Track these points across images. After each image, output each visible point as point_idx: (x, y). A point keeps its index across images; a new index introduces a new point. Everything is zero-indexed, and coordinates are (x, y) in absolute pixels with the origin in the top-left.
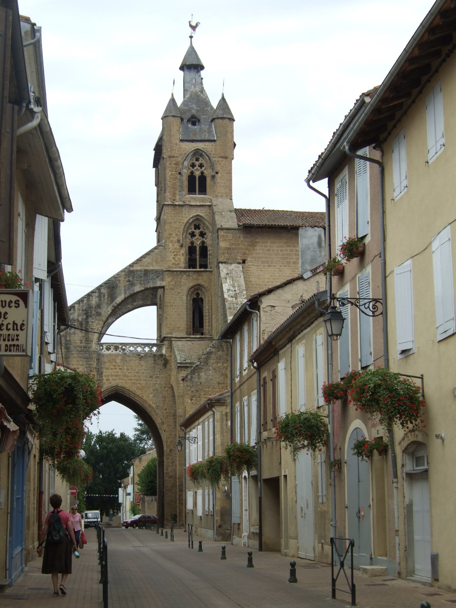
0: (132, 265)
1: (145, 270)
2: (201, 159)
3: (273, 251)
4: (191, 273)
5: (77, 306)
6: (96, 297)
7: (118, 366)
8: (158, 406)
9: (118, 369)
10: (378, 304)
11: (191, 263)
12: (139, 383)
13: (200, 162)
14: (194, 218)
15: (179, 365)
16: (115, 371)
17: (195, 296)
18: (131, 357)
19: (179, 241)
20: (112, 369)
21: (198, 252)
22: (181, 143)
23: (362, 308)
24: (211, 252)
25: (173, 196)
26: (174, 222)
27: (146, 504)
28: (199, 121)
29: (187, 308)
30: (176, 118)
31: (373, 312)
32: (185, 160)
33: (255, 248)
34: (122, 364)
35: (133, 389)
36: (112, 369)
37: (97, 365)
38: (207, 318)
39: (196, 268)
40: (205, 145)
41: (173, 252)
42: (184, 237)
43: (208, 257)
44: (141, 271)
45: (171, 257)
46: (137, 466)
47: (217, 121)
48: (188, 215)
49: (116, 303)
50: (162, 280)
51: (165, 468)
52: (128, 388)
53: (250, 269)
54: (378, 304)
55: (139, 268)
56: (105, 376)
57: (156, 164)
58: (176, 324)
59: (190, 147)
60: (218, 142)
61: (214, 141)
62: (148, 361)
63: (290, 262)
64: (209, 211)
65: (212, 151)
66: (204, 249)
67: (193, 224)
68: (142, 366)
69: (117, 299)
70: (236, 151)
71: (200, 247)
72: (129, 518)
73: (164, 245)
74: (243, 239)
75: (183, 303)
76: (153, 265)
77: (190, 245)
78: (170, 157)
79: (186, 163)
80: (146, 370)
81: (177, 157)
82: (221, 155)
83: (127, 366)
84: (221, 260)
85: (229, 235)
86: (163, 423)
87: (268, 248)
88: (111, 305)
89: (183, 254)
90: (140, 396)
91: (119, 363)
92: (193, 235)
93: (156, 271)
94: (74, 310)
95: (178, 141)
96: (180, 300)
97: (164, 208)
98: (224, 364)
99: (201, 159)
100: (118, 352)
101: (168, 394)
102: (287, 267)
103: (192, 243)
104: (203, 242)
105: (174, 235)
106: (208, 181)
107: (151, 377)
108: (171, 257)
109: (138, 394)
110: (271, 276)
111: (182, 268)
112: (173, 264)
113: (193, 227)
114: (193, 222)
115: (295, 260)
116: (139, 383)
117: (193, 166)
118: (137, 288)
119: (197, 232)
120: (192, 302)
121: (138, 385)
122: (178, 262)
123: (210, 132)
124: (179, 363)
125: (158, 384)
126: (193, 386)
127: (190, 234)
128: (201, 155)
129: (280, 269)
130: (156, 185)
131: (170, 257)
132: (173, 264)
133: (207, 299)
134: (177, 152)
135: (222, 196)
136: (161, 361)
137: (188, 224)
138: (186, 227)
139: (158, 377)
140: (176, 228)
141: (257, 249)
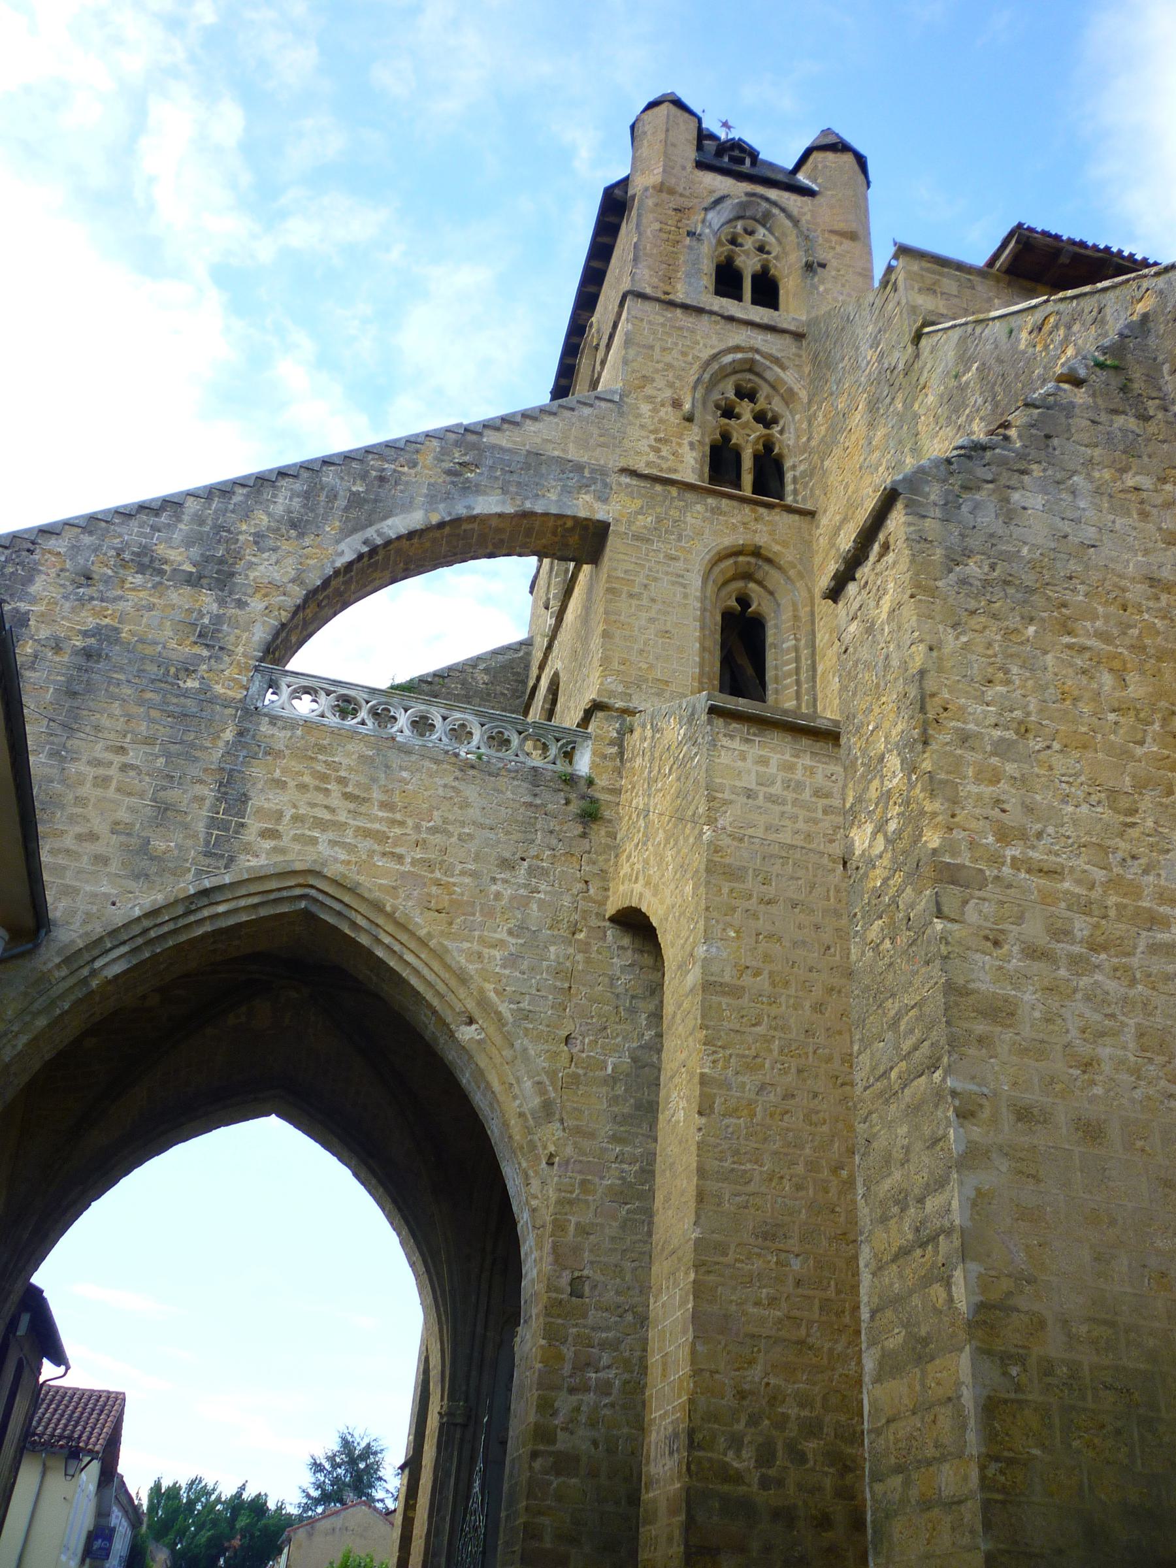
5: (192, 506)
7: (342, 781)
16: (320, 798)
29: (702, 620)
34: (363, 780)
35: (405, 905)
36: (303, 787)
46: (300, 1546)
49: (379, 534)
52: (377, 895)
56: (259, 811)
58: (651, 667)
62: (499, 791)
67: (733, 378)
68: (464, 805)
69: (389, 522)
75: (686, 596)
80: (482, 826)
82: (836, 228)
89: (691, 444)
90: (432, 943)
92: (729, 413)
96: (674, 583)
100: (351, 722)
101: (588, 961)
107: (507, 864)
109: (422, 933)
120: (719, 618)
125: (541, 902)
133: (786, 615)
139: (545, 873)
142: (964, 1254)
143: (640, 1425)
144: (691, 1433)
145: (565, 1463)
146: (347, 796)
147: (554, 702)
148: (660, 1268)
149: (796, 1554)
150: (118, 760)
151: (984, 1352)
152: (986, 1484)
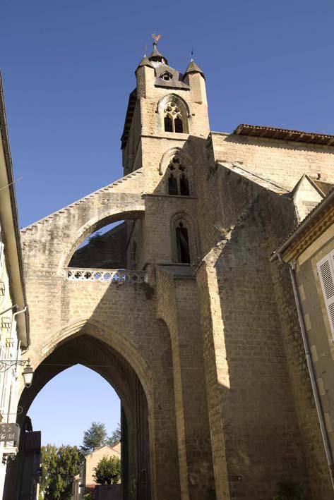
7: (90, 295)
16: (86, 301)
17: (178, 226)
62: (127, 291)
88: (83, 227)
94: (37, 230)
98: (262, 245)
142: (222, 417)
143: (176, 441)
144: (186, 440)
145: (162, 445)
146: (92, 299)
147: (135, 247)
148: (177, 405)
149: (77, 477)
150: (37, 300)
151: (226, 433)
152: (226, 454)
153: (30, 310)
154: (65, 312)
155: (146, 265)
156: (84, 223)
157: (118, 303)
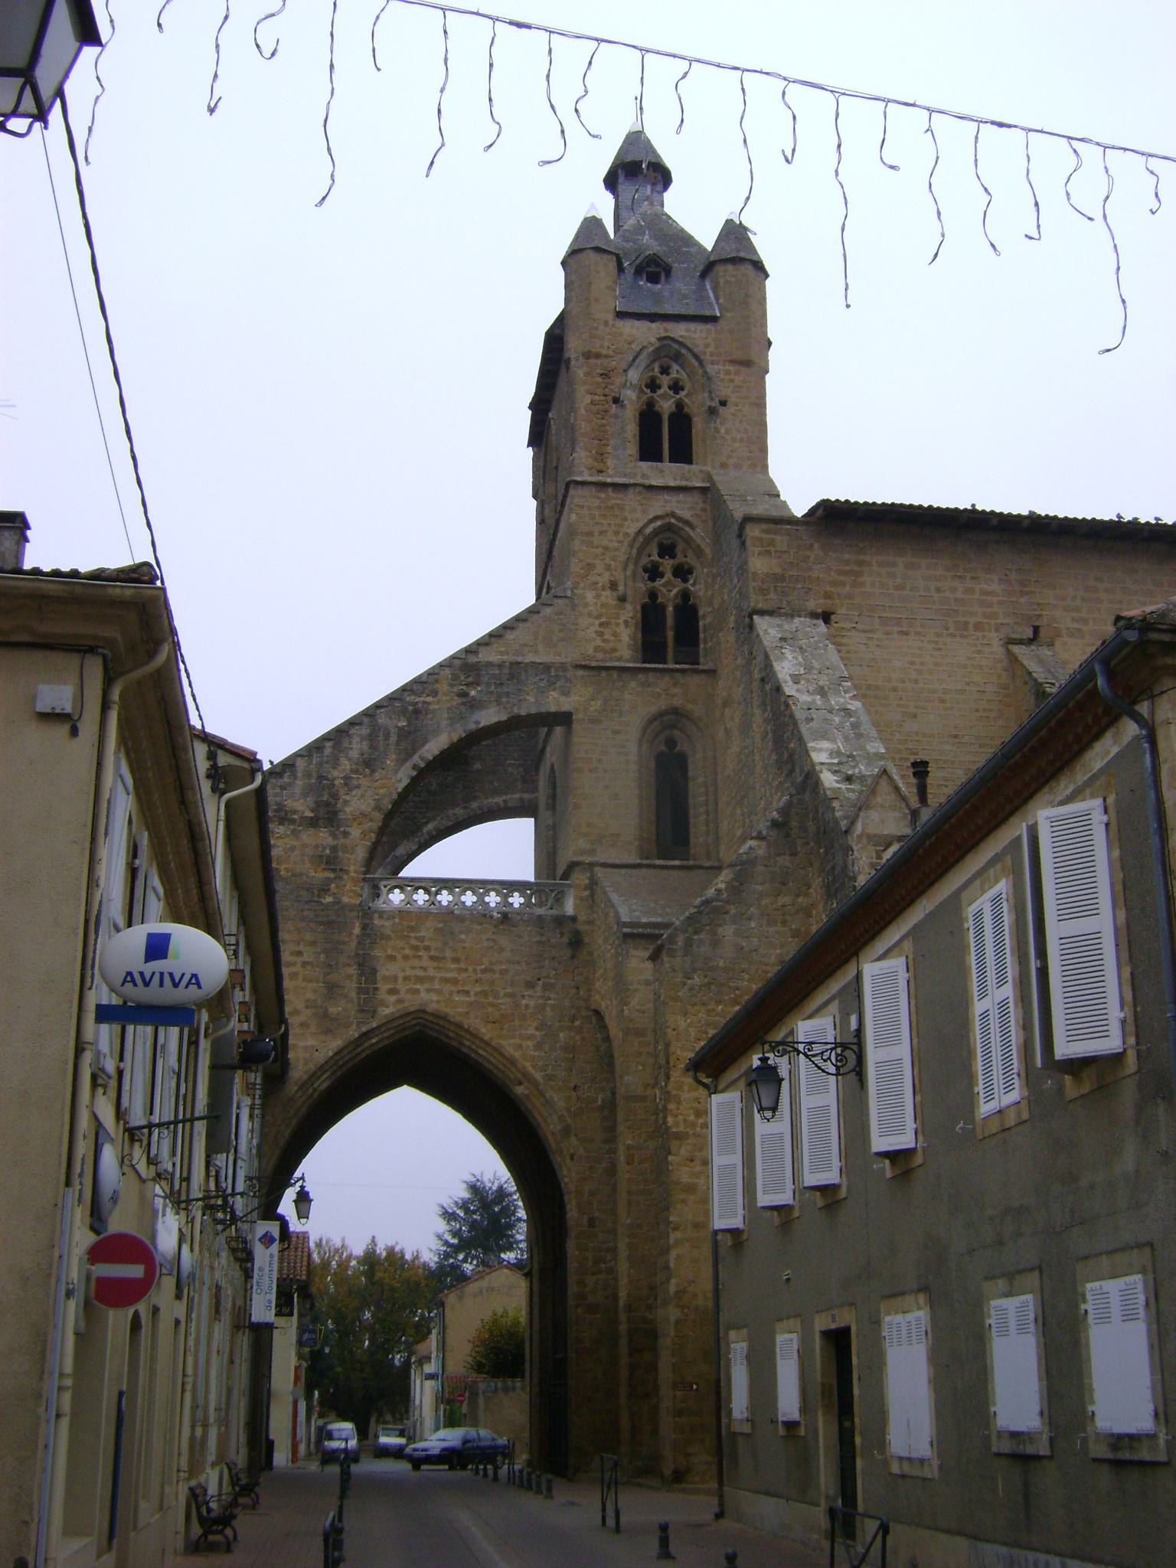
0: (474, 648)
1: (511, 664)
2: (675, 367)
3: (912, 589)
4: (651, 677)
5: (301, 764)
6: (363, 739)
7: (427, 948)
8: (550, 1078)
9: (425, 958)
10: (848, 1053)
11: (651, 648)
12: (492, 1005)
13: (674, 375)
14: (659, 523)
15: (625, 930)
16: (417, 963)
17: (663, 748)
18: (467, 923)
19: (613, 586)
20: (406, 957)
21: (670, 621)
22: (620, 323)
23: (818, 1060)
24: (709, 619)
25: (596, 460)
26: (601, 533)
27: (481, 1400)
28: (668, 271)
30: (606, 257)
31: (838, 1068)
32: (631, 365)
33: (860, 580)
36: (406, 957)
37: (359, 943)
38: (702, 810)
39: (665, 663)
40: (688, 330)
41: (598, 617)
42: (629, 573)
43: (701, 636)
44: (500, 666)
45: (592, 629)
47: (720, 269)
48: (638, 515)
49: (422, 759)
50: (566, 693)
51: (572, 1280)
52: (458, 1019)
53: (845, 641)
54: (848, 1053)
55: (495, 658)
56: (385, 978)
57: (538, 437)
59: (646, 334)
60: (722, 323)
61: (713, 319)
62: (520, 936)
63: (967, 623)
64: (701, 505)
65: (707, 346)
66: (688, 612)
67: (656, 540)
69: (426, 747)
70: (772, 354)
71: (676, 607)
72: (438, 1439)
73: (569, 593)
74: (821, 553)
76: (536, 652)
77: (647, 600)
78: (587, 355)
79: (634, 375)
80: (512, 963)
81: (606, 356)
82: (735, 357)
83: (454, 950)
84: (756, 601)
85: (778, 538)
86: (566, 1131)
87: (899, 580)
88: (409, 764)
89: (626, 622)
90: (493, 1044)
91: (431, 939)
92: (654, 572)
93: (547, 667)
94: (294, 775)
95: (610, 317)
97: (572, 492)
98: (800, 899)
99: (675, 367)
101: (583, 1039)
102: (958, 639)
103: (653, 595)
104: (685, 595)
105: (600, 568)
106: (698, 424)
108: (592, 629)
109: (487, 1038)
110: (912, 663)
111: (629, 661)
112: (596, 649)
113: (655, 550)
114: (657, 532)
115: (979, 619)
116: (492, 1005)
117: (653, 385)
118: (489, 716)
119: (667, 565)
121: (490, 1009)
122: (611, 645)
123: (701, 297)
124: (625, 925)
126: (695, 970)
127: (645, 570)
128: (677, 357)
129: (937, 643)
130: (535, 496)
131: (588, 628)
132: (596, 649)
134: (606, 344)
135: (738, 466)
136: (562, 934)
137: (641, 539)
138: (637, 545)
139: (552, 986)
140: (606, 548)
141: (862, 584)
146: (432, 958)
150: (299, 960)
153: (291, 1032)
154: (366, 991)
155: (573, 866)
156: (409, 755)
157: (497, 968)
